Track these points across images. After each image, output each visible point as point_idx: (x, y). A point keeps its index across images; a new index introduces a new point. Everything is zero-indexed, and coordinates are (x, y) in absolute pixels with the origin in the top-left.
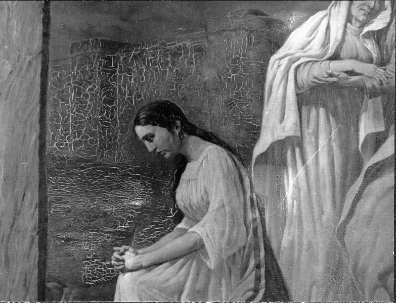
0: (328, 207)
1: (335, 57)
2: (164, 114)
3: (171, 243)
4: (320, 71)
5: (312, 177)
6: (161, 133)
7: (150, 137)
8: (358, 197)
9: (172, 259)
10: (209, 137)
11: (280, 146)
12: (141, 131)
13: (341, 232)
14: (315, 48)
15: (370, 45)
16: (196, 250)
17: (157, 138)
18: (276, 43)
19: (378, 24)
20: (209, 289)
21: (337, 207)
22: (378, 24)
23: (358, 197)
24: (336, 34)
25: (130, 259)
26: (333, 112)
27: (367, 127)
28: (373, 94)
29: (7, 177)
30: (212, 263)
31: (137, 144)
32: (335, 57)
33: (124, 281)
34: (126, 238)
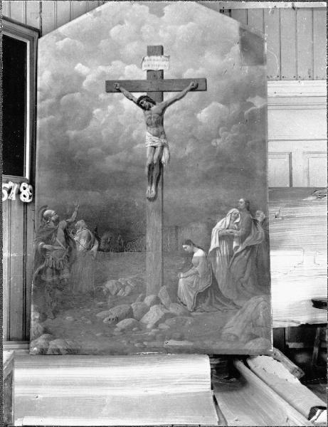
0: (226, 263)
1: (228, 229)
2: (188, 242)
3: (191, 271)
4: (224, 232)
5: (293, 107)
6: (188, 247)
7: (186, 248)
8: (233, 261)
9: (191, 275)
10: (199, 248)
11: (215, 249)
12: (184, 246)
13: (229, 269)
14: (223, 227)
15: (235, 225)
16: (197, 273)
17: (187, 248)
18: (214, 225)
19: (237, 221)
20: (4, 220)
21: (228, 263)
22: (237, 221)
23: (233, 261)
24: (228, 223)
25: (182, 275)
26: (227, 241)
27: (235, 244)
28: (236, 237)
29: (96, 230)
30: (200, 276)
31: (182, 249)
32: (228, 229)
33: (181, 280)
34: (181, 270)
